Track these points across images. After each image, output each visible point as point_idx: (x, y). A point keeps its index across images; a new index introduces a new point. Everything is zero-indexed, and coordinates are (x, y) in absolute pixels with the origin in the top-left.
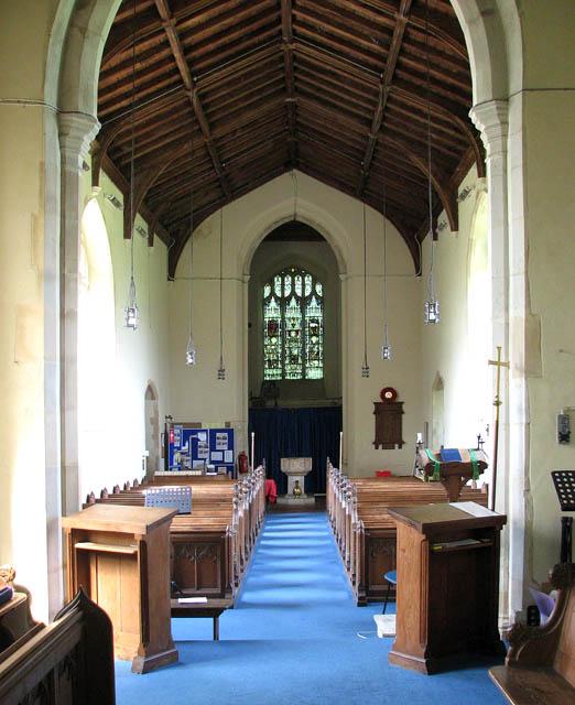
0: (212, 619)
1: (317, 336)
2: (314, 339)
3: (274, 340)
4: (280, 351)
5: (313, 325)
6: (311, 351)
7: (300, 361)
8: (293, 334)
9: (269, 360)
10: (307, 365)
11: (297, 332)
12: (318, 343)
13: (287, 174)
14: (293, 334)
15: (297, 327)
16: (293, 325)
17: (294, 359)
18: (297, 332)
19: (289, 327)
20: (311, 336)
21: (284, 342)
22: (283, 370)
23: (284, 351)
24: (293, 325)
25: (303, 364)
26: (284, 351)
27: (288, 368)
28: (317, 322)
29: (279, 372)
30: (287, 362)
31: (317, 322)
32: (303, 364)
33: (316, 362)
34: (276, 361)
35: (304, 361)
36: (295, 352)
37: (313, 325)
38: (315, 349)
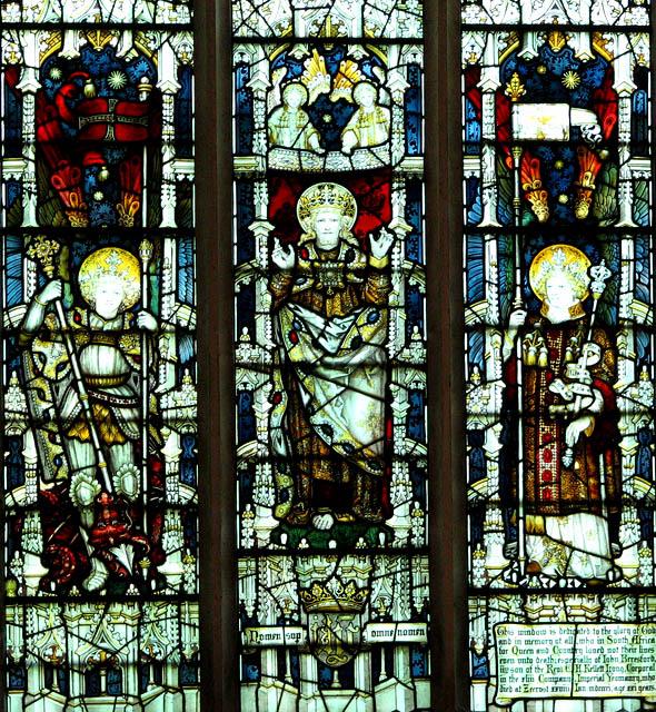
0: (420, 36)
1: (594, 239)
2: (561, 280)
3: (110, 281)
4: (182, 401)
5: (541, 121)
6: (529, 408)
7: (404, 522)
8: (327, 218)
9: (57, 507)
10: (491, 560)
11: (368, 189)
12: (598, 319)
13: (547, 137)
14: (327, 218)
15: (373, 134)
16: (329, 118)
17: (337, 493)
18: (368, 189)
19: (287, 137)
20: (525, 241)
21: (222, 310)
22: (217, 602)
23: (223, 411)
24: (329, 118)
25: (445, 551)
26: (223, 411)
27: (269, 591)
28: (599, 97)
29: (175, 634)
30: (260, 523)
31: (599, 97)
32: (445, 551)
33: (585, 531)
34: (137, 517)
35: (454, 527)
36: (353, 417)
37: (541, 121)
38: (575, 390)
